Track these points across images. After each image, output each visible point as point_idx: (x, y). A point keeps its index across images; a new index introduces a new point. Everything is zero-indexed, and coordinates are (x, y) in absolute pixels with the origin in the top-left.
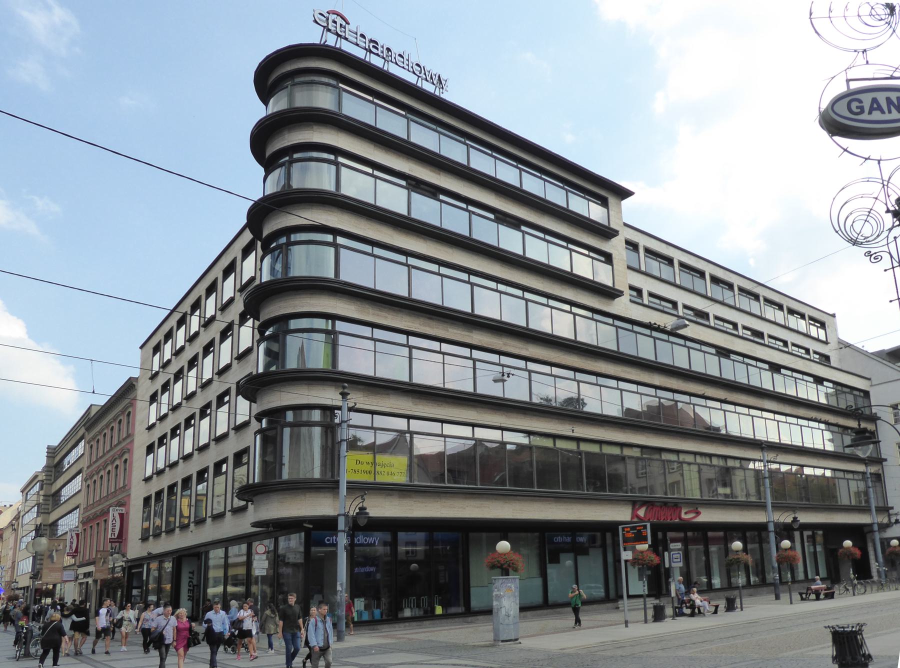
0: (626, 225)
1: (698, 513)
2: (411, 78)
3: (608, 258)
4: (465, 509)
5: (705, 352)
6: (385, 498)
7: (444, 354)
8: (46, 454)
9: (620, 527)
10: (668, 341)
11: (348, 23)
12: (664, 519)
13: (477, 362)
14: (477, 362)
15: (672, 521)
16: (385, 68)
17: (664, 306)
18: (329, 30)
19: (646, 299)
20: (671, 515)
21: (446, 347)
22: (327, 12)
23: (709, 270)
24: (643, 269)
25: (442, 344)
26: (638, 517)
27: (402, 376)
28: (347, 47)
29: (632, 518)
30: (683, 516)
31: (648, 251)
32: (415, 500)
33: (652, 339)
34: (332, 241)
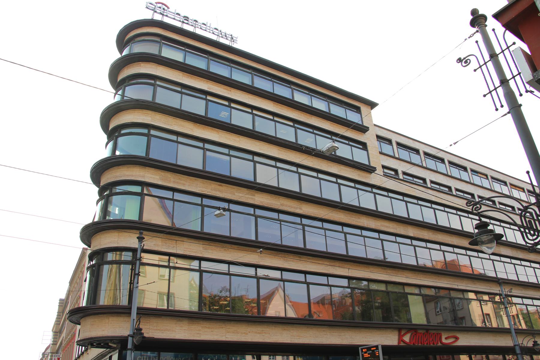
0: (375, 125)
1: (457, 339)
2: (214, 37)
3: (364, 146)
4: (247, 334)
5: (447, 212)
6: (176, 324)
7: (326, 229)
8: (59, 302)
9: (360, 348)
10: (417, 204)
11: (168, 8)
12: (427, 344)
13: (347, 235)
14: (347, 235)
15: (428, 345)
16: (218, 40)
17: (416, 182)
18: (156, 12)
19: (401, 176)
20: (432, 340)
21: (326, 225)
22: (155, 3)
23: (422, 148)
24: (397, 156)
25: (175, 193)
26: (404, 342)
27: (196, 227)
28: (166, 20)
29: (399, 343)
30: (444, 341)
31: (399, 144)
32: (202, 326)
33: (404, 203)
34: (252, 159)
